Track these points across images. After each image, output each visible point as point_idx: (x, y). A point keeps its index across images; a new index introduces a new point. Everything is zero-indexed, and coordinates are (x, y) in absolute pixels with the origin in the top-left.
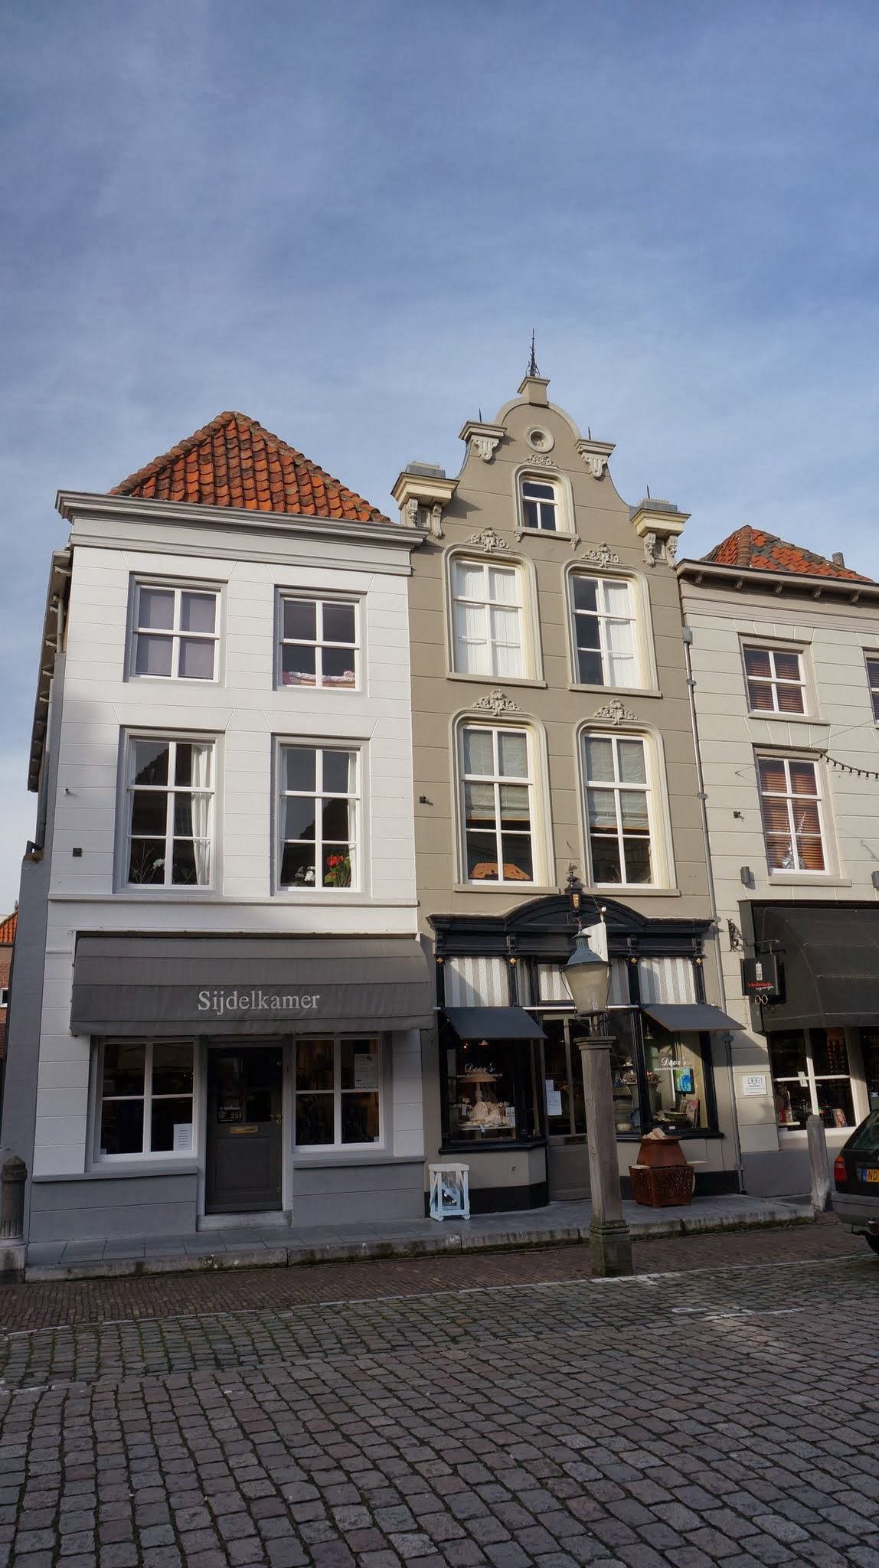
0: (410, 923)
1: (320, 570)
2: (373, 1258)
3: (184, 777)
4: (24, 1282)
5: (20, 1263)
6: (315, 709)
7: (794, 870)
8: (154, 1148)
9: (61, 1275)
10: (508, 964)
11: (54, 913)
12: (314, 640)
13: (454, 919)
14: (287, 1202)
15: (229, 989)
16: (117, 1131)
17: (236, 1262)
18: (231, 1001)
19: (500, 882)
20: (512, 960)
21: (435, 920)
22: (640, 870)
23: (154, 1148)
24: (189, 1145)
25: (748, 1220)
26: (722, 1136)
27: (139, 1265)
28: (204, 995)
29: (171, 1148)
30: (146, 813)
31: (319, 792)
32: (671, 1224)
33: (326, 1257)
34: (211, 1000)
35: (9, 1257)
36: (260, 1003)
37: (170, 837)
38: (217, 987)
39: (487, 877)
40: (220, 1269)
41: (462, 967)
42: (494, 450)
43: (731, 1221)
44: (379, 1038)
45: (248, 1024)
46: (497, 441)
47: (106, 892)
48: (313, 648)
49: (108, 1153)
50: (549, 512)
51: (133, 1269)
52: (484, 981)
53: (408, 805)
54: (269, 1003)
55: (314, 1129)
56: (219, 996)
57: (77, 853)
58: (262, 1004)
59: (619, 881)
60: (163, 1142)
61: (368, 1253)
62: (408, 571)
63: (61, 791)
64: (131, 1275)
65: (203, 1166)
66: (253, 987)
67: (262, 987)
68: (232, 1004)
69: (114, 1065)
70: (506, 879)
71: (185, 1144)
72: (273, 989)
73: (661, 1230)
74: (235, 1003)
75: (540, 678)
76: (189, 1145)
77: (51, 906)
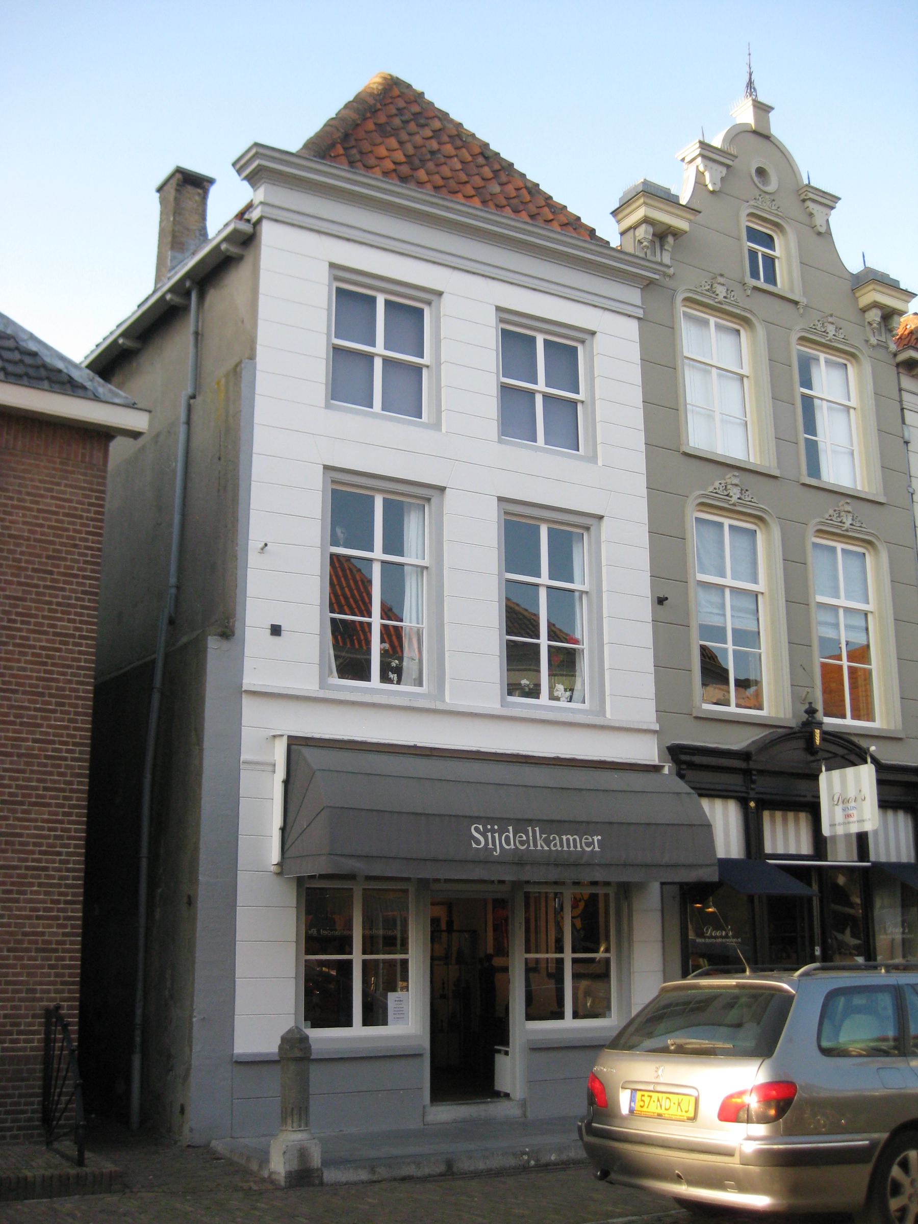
0: (647, 751)
3: (394, 543)
4: (322, 1184)
5: (316, 1161)
6: (545, 476)
8: (366, 1023)
9: (364, 1176)
11: (250, 710)
12: (539, 379)
16: (325, 1000)
17: (553, 1158)
18: (507, 838)
19: (732, 709)
22: (863, 710)
27: (449, 1164)
28: (477, 829)
30: (346, 585)
31: (544, 579)
35: (303, 1154)
36: (537, 842)
37: (376, 621)
40: (536, 1166)
41: (712, 809)
44: (611, 891)
47: (309, 685)
49: (313, 1027)
51: (442, 1168)
53: (645, 609)
54: (547, 842)
55: (545, 1007)
57: (276, 630)
59: (843, 716)
60: (375, 1014)
63: (254, 544)
64: (441, 1175)
65: (426, 1044)
66: (530, 822)
67: (539, 822)
68: (508, 843)
69: (322, 912)
71: (402, 1016)
75: (774, 463)
77: (246, 701)
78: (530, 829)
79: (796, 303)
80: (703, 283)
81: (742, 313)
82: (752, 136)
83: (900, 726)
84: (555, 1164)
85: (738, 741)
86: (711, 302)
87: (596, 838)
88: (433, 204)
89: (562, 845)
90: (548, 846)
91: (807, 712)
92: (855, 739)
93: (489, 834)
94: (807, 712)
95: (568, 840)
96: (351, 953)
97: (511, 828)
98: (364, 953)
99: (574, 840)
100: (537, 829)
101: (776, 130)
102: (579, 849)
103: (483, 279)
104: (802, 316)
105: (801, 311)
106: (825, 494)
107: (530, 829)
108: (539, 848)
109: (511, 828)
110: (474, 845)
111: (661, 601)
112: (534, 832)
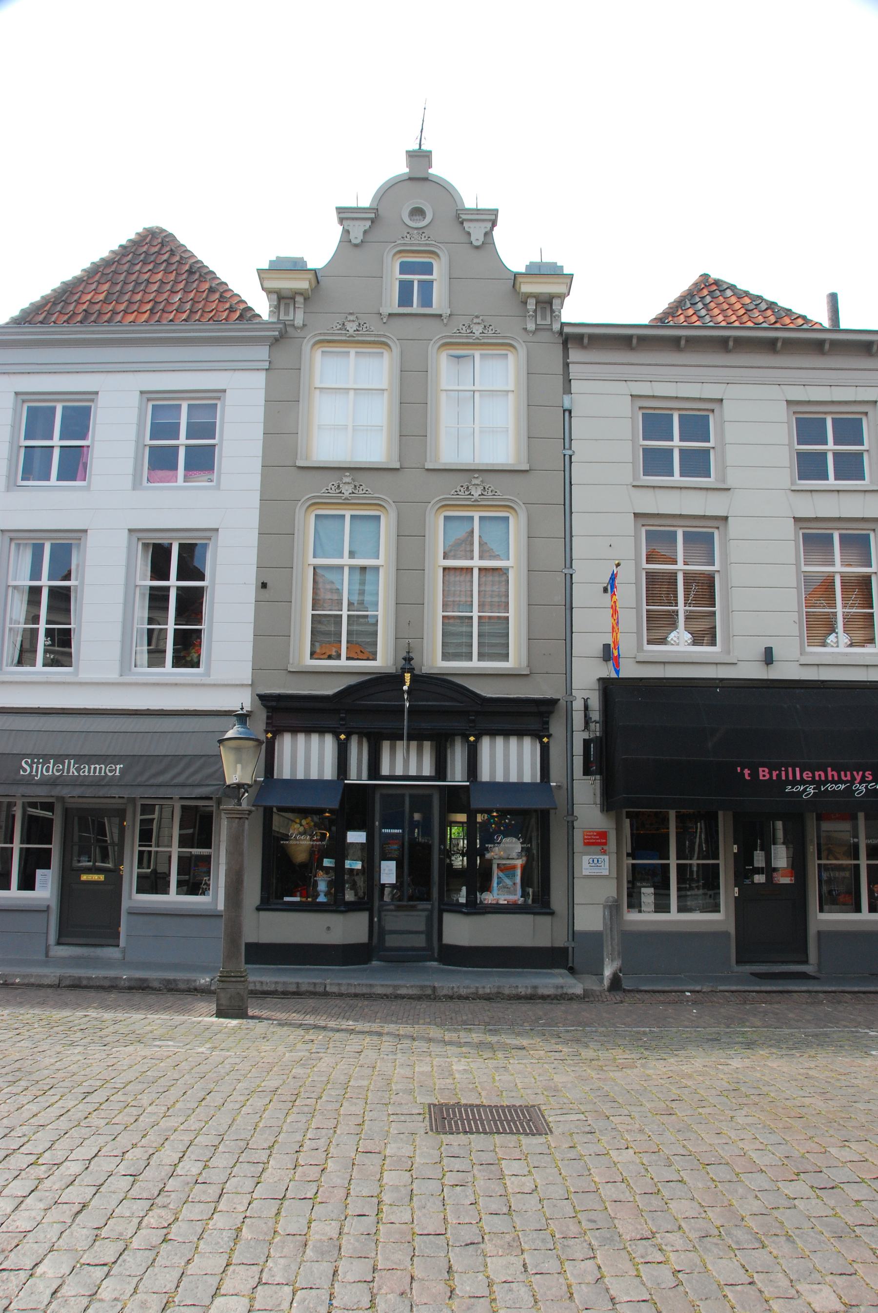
1: (183, 377)
2: (130, 988)
6: (177, 507)
7: (839, 645)
8: (20, 888)
10: (338, 739)
12: (180, 445)
13: (280, 698)
14: (122, 942)
15: (46, 758)
18: (48, 767)
20: (343, 737)
21: (263, 698)
23: (20, 888)
24: (46, 888)
25: (507, 991)
26: (552, 914)
28: (26, 763)
29: (34, 889)
32: (422, 987)
33: (91, 984)
34: (32, 768)
38: (38, 756)
39: (330, 657)
42: (365, 232)
43: (488, 991)
45: (59, 788)
46: (369, 223)
47: (113, 675)
48: (177, 447)
50: (426, 287)
52: (309, 757)
53: (250, 592)
54: (78, 770)
55: (154, 882)
56: (33, 762)
58: (73, 771)
60: (27, 883)
61: (127, 984)
62: (266, 365)
66: (68, 756)
67: (73, 756)
68: (47, 771)
70: (348, 658)
72: (81, 759)
73: (411, 992)
74: (51, 770)
76: (46, 888)
78: (67, 761)
79: (441, 316)
80: (461, 326)
81: (376, 339)
82: (408, 183)
83: (524, 663)
84: (18, 984)
85: (329, 688)
86: (344, 338)
87: (118, 767)
88: (81, 332)
89: (89, 772)
90: (78, 772)
91: (405, 659)
92: (445, 677)
93: (35, 766)
94: (405, 659)
95: (95, 768)
96: (668, 859)
97: (52, 761)
98: (678, 859)
99: (101, 768)
100: (72, 761)
101: (436, 170)
102: (103, 774)
103: (6, 376)
104: (446, 325)
105: (445, 321)
106: (314, 472)
107: (67, 761)
108: (71, 774)
109: (52, 761)
110: (22, 773)
111: (264, 585)
112: (69, 763)
